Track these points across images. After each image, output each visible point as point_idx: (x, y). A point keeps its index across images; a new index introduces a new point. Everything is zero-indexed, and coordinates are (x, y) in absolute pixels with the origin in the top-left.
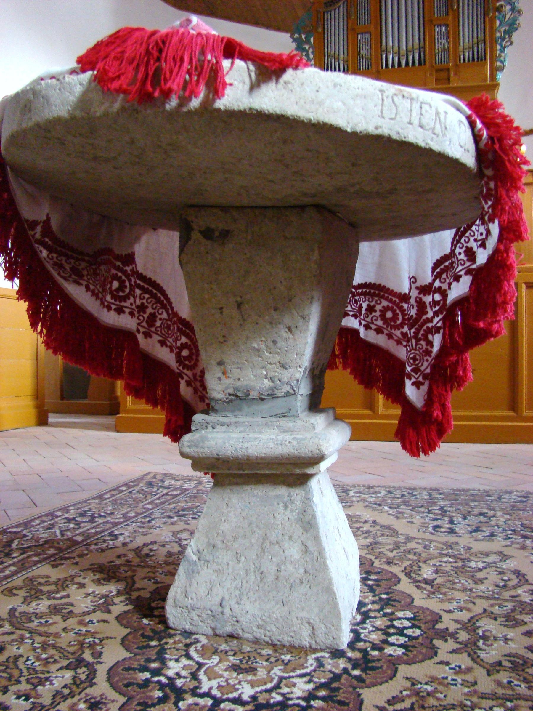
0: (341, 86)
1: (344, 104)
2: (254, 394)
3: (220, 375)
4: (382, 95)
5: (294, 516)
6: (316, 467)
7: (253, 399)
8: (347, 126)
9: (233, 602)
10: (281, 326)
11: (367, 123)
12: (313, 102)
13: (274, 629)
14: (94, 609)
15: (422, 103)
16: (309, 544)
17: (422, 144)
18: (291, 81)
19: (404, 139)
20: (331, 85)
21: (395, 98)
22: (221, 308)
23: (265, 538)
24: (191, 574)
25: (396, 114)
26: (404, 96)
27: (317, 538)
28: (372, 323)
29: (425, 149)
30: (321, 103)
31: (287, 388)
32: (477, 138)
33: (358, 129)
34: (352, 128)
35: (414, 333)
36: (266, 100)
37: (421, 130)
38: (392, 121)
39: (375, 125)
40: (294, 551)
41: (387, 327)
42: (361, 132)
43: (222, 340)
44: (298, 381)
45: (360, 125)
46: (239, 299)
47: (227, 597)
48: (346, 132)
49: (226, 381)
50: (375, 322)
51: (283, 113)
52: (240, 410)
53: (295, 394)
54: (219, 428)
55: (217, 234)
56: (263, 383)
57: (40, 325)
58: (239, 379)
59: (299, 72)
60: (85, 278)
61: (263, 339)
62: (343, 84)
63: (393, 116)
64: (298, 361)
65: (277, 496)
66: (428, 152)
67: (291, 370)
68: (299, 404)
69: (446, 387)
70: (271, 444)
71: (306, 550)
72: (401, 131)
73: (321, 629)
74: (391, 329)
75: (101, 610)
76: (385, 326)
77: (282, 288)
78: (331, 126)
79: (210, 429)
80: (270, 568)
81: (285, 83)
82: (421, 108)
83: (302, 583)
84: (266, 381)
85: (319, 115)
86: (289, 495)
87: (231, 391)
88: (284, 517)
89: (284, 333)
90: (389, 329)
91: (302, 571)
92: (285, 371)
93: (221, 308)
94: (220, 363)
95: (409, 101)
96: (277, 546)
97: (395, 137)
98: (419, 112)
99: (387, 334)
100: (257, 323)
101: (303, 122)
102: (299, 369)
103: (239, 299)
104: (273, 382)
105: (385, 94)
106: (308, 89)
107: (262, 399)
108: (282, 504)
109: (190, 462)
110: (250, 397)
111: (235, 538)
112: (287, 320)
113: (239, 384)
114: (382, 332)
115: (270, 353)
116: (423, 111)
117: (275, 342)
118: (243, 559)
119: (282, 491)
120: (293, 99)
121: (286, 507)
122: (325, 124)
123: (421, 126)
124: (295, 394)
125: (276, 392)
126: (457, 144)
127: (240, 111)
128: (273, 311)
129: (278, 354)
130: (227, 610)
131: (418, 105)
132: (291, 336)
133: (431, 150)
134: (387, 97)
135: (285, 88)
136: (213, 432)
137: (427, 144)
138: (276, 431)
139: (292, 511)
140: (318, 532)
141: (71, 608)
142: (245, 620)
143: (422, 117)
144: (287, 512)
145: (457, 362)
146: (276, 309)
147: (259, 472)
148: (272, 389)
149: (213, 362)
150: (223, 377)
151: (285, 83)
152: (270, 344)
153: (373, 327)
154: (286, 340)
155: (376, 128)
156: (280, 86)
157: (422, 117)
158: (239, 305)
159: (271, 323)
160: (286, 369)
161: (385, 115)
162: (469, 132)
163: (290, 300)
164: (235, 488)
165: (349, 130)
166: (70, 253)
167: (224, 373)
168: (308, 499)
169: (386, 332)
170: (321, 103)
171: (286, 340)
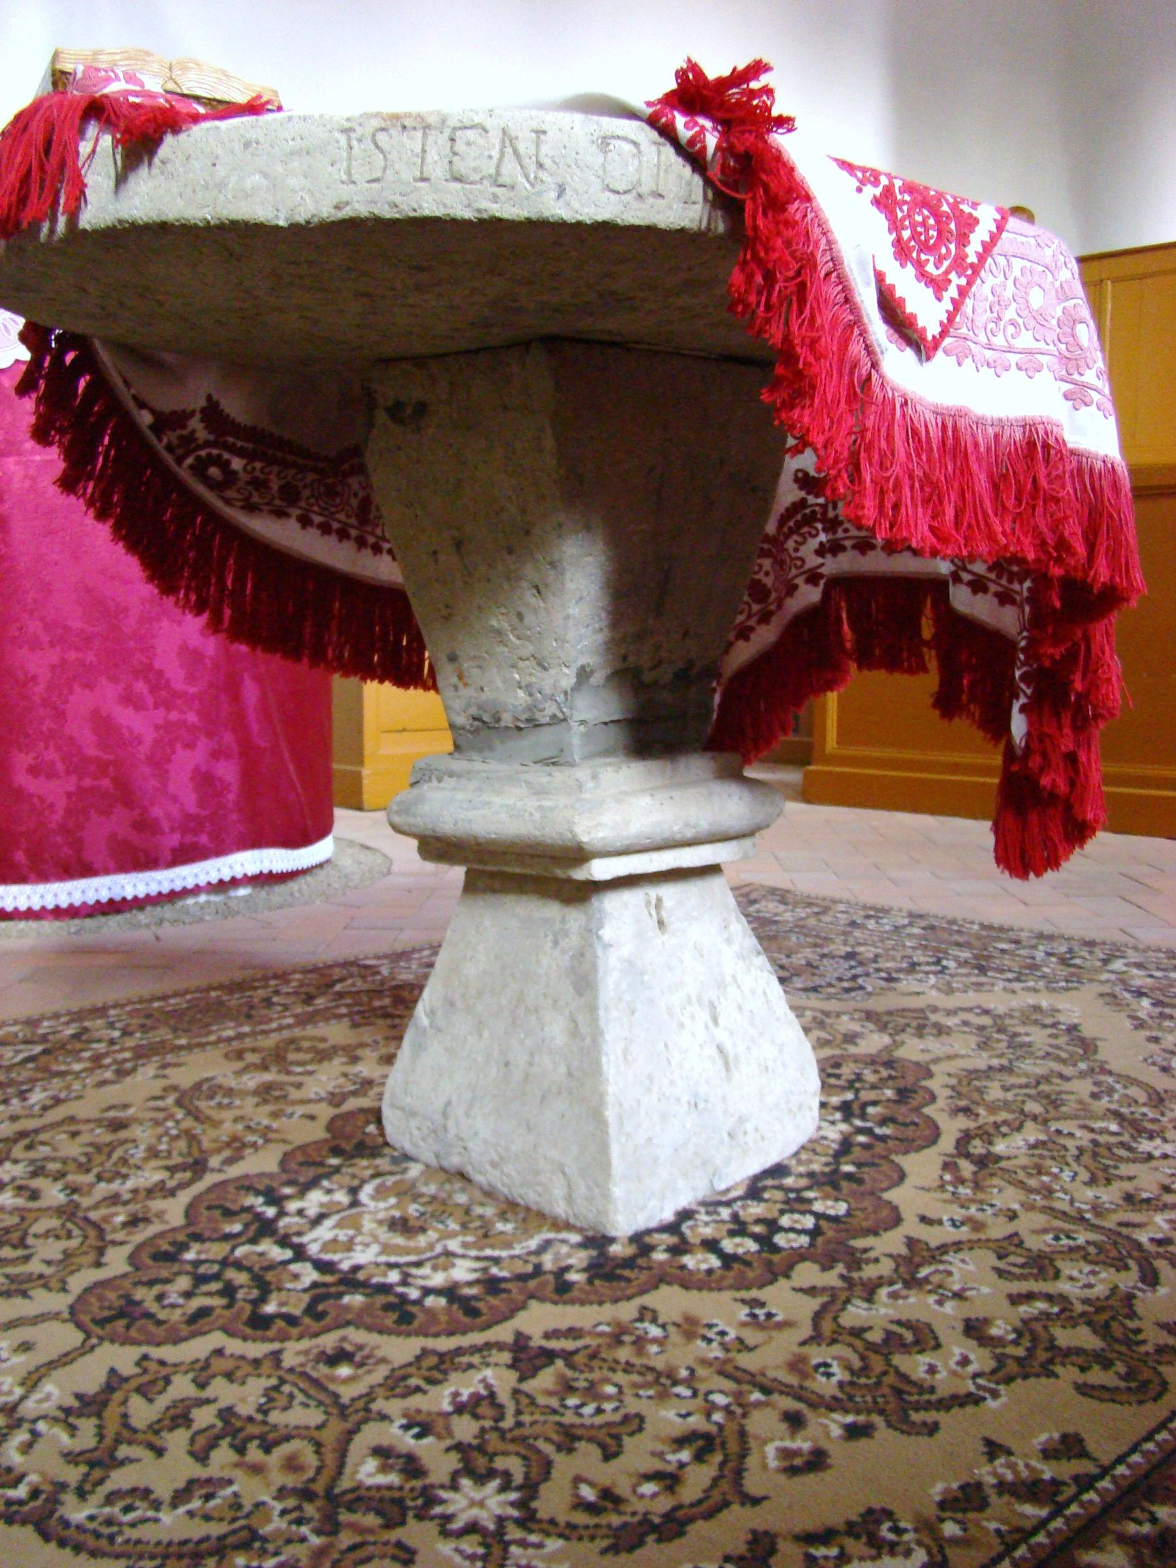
0: (257, 143)
1: (266, 176)
2: (507, 719)
3: (455, 680)
4: (349, 139)
5: (565, 961)
6: (585, 866)
7: (507, 728)
8: (277, 217)
9: (461, 1111)
10: (524, 584)
11: (316, 201)
12: (206, 187)
13: (514, 1174)
14: (946, 1253)
15: (455, 129)
16: (580, 1019)
17: (468, 214)
18: (171, 156)
19: (412, 214)
20: (238, 147)
21: (382, 138)
22: (435, 553)
23: (520, 998)
24: (419, 1048)
25: (385, 169)
26: (404, 127)
27: (593, 1009)
28: (965, 569)
29: (481, 221)
30: (221, 186)
31: (550, 709)
32: (692, 155)
33: (301, 218)
34: (287, 219)
35: (1029, 589)
36: (137, 201)
37: (457, 186)
38: (374, 185)
39: (335, 202)
40: (556, 1030)
41: (999, 576)
42: (308, 222)
43: (444, 612)
44: (566, 693)
45: (302, 209)
46: (454, 532)
47: (454, 1098)
48: (277, 228)
49: (465, 692)
50: (969, 567)
51: (164, 218)
52: (491, 748)
53: (565, 720)
54: (449, 782)
55: (409, 411)
56: (516, 698)
57: (929, 601)
58: (482, 689)
59: (183, 136)
60: (303, 504)
61: (503, 610)
62: (262, 140)
63: (379, 174)
64: (560, 653)
65: (545, 921)
66: (492, 226)
67: (552, 672)
68: (576, 741)
69: (1059, 720)
70: (503, 816)
71: (574, 1032)
72: (398, 199)
73: (581, 1189)
74: (1010, 581)
75: (929, 1249)
76: (993, 576)
77: (514, 510)
78: (246, 224)
79: (435, 783)
80: (520, 1058)
81: (163, 162)
82: (453, 140)
83: (560, 1093)
84: (521, 693)
85: (218, 209)
86: (563, 921)
87: (474, 711)
88: (551, 961)
89: (531, 598)
90: (1004, 582)
91: (563, 1069)
92: (545, 674)
93: (435, 553)
94: (453, 658)
95: (419, 134)
96: (533, 1018)
97: (387, 213)
98: (448, 151)
99: (997, 594)
100: (488, 580)
101: (196, 226)
102: (566, 670)
103: (454, 532)
104: (530, 695)
105: (353, 135)
106: (197, 165)
107: (519, 729)
108: (551, 937)
109: (414, 843)
110: (503, 724)
111: (480, 993)
112: (529, 570)
113: (484, 697)
114: (985, 590)
115: (519, 638)
116: (460, 147)
117: (520, 616)
118: (486, 1033)
119: (552, 910)
120: (175, 190)
121: (556, 943)
122: (234, 223)
123: (458, 179)
124: (565, 720)
125: (538, 715)
126: (597, 186)
127: (108, 228)
128: (507, 557)
129: (528, 639)
130: (451, 1123)
131: (443, 139)
132: (542, 605)
133: (500, 220)
134: (360, 141)
135: (162, 173)
136: (437, 788)
137: (479, 211)
138: (523, 791)
139: (563, 952)
140: (596, 997)
141: (1001, 1265)
142: (475, 1146)
143: (456, 159)
144: (556, 953)
145: (1071, 657)
146: (510, 551)
147: (506, 869)
148: (530, 708)
149: (442, 656)
150: (460, 685)
151: (163, 162)
152: (515, 620)
153: (966, 577)
154: (536, 611)
155: (337, 207)
156: (155, 171)
157: (456, 159)
158: (458, 545)
159: (508, 578)
160: (545, 669)
161: (355, 177)
162: (669, 151)
163: (528, 533)
164: (491, 899)
165: (282, 223)
166: (300, 461)
167: (460, 677)
168: (591, 932)
169: (993, 588)
170: (221, 186)
171: (536, 611)
